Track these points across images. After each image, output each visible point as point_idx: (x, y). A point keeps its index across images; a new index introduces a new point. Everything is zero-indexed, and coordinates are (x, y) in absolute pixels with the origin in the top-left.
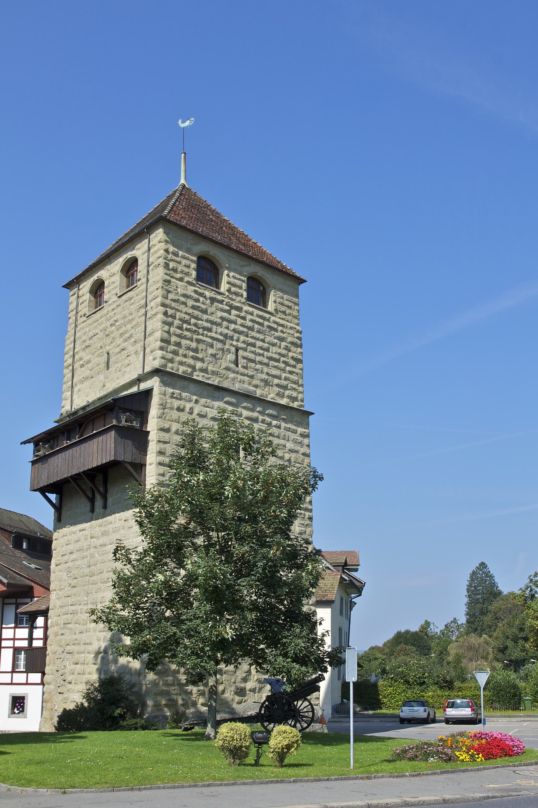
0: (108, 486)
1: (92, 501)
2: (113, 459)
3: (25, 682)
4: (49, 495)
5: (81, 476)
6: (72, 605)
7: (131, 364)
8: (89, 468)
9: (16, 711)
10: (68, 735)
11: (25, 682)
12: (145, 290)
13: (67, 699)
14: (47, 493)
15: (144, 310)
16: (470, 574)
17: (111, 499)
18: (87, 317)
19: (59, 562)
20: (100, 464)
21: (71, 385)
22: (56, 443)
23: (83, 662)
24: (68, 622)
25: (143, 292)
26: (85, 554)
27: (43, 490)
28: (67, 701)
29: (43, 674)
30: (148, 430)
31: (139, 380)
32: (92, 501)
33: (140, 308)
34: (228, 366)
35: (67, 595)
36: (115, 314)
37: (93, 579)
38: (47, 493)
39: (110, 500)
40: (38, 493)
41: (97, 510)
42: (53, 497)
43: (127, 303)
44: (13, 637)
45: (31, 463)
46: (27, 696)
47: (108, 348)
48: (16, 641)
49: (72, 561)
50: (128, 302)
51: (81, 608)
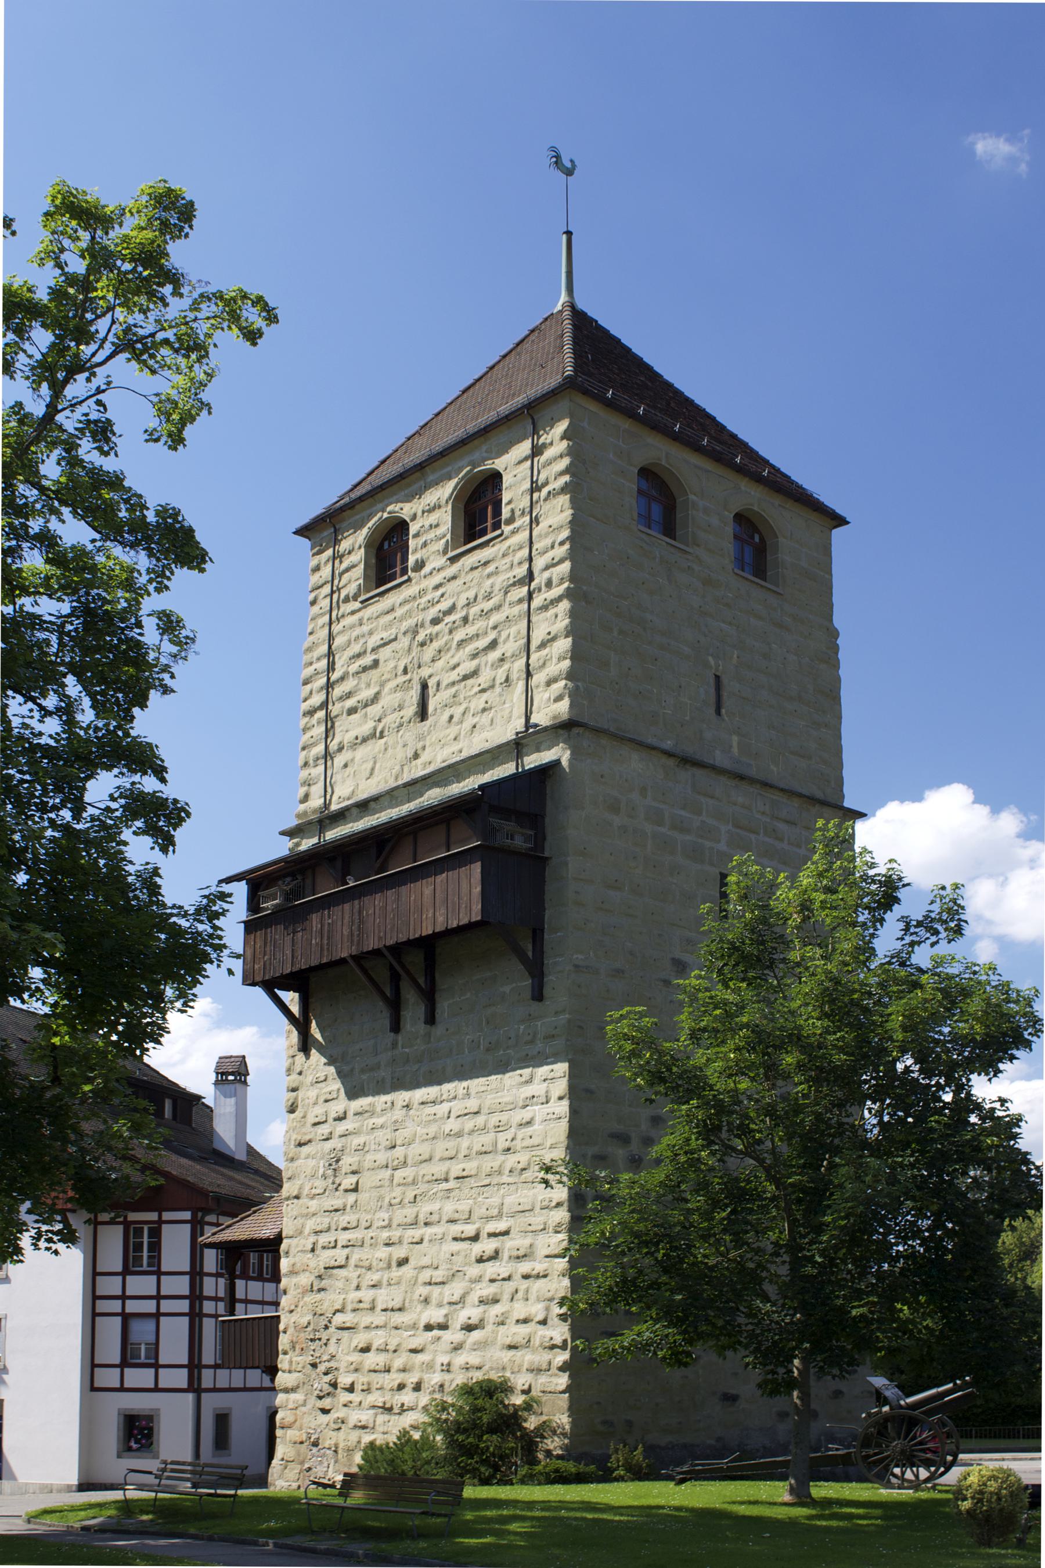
0: (437, 975)
1: (395, 1006)
2: (479, 918)
3: (118, 1385)
4: (281, 994)
5: (383, 955)
6: (345, 1229)
7: (491, 708)
8: (411, 938)
9: (134, 1446)
10: (605, 1516)
11: (152, 1386)
12: (528, 543)
13: (343, 1422)
14: (276, 990)
15: (526, 588)
16: (1027, 1153)
17: (446, 1004)
18: (362, 602)
19: (307, 1138)
20: (443, 929)
21: (323, 752)
22: (309, 881)
23: (382, 1347)
24: (337, 1264)
25: (521, 548)
26: (379, 1121)
27: (270, 986)
28: (343, 1426)
29: (216, 1366)
30: (546, 854)
31: (518, 747)
32: (395, 1006)
33: (514, 584)
34: (551, 714)
35: (332, 1208)
36: (442, 596)
37: (404, 1175)
38: (276, 990)
39: (444, 1006)
40: (259, 992)
41: (408, 1026)
42: (291, 998)
43: (476, 573)
44: (120, 1293)
45: (242, 925)
46: (159, 1415)
47: (425, 672)
48: (128, 1302)
49: (341, 1136)
50: (480, 569)
51: (373, 1234)
